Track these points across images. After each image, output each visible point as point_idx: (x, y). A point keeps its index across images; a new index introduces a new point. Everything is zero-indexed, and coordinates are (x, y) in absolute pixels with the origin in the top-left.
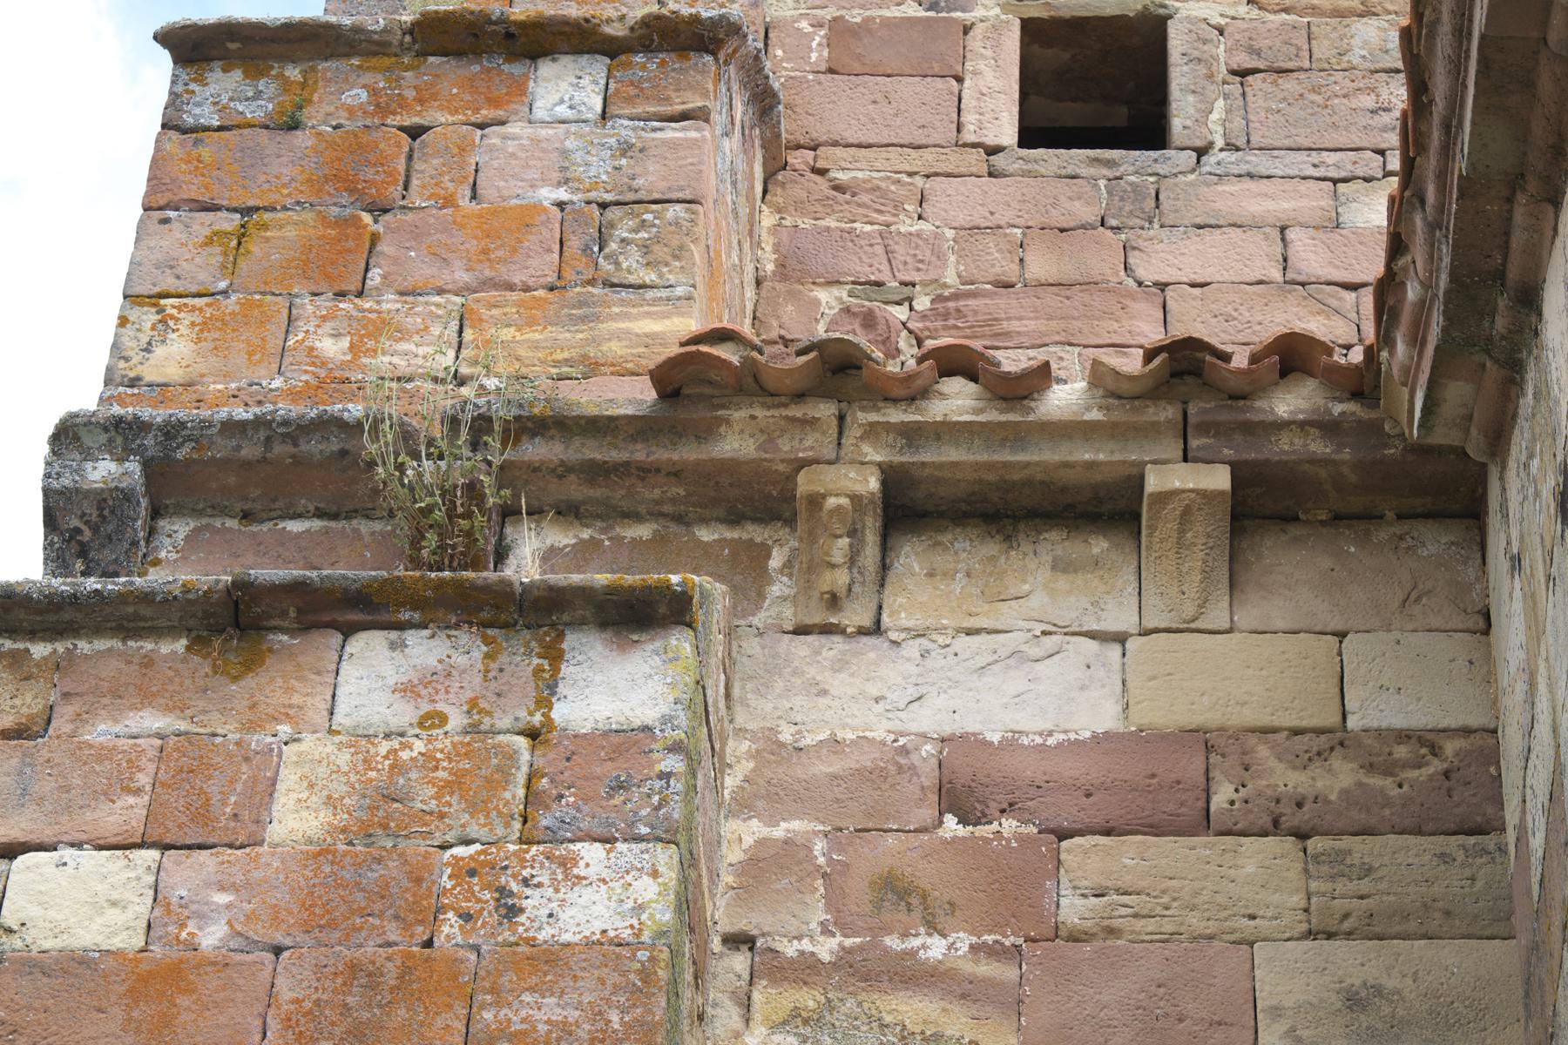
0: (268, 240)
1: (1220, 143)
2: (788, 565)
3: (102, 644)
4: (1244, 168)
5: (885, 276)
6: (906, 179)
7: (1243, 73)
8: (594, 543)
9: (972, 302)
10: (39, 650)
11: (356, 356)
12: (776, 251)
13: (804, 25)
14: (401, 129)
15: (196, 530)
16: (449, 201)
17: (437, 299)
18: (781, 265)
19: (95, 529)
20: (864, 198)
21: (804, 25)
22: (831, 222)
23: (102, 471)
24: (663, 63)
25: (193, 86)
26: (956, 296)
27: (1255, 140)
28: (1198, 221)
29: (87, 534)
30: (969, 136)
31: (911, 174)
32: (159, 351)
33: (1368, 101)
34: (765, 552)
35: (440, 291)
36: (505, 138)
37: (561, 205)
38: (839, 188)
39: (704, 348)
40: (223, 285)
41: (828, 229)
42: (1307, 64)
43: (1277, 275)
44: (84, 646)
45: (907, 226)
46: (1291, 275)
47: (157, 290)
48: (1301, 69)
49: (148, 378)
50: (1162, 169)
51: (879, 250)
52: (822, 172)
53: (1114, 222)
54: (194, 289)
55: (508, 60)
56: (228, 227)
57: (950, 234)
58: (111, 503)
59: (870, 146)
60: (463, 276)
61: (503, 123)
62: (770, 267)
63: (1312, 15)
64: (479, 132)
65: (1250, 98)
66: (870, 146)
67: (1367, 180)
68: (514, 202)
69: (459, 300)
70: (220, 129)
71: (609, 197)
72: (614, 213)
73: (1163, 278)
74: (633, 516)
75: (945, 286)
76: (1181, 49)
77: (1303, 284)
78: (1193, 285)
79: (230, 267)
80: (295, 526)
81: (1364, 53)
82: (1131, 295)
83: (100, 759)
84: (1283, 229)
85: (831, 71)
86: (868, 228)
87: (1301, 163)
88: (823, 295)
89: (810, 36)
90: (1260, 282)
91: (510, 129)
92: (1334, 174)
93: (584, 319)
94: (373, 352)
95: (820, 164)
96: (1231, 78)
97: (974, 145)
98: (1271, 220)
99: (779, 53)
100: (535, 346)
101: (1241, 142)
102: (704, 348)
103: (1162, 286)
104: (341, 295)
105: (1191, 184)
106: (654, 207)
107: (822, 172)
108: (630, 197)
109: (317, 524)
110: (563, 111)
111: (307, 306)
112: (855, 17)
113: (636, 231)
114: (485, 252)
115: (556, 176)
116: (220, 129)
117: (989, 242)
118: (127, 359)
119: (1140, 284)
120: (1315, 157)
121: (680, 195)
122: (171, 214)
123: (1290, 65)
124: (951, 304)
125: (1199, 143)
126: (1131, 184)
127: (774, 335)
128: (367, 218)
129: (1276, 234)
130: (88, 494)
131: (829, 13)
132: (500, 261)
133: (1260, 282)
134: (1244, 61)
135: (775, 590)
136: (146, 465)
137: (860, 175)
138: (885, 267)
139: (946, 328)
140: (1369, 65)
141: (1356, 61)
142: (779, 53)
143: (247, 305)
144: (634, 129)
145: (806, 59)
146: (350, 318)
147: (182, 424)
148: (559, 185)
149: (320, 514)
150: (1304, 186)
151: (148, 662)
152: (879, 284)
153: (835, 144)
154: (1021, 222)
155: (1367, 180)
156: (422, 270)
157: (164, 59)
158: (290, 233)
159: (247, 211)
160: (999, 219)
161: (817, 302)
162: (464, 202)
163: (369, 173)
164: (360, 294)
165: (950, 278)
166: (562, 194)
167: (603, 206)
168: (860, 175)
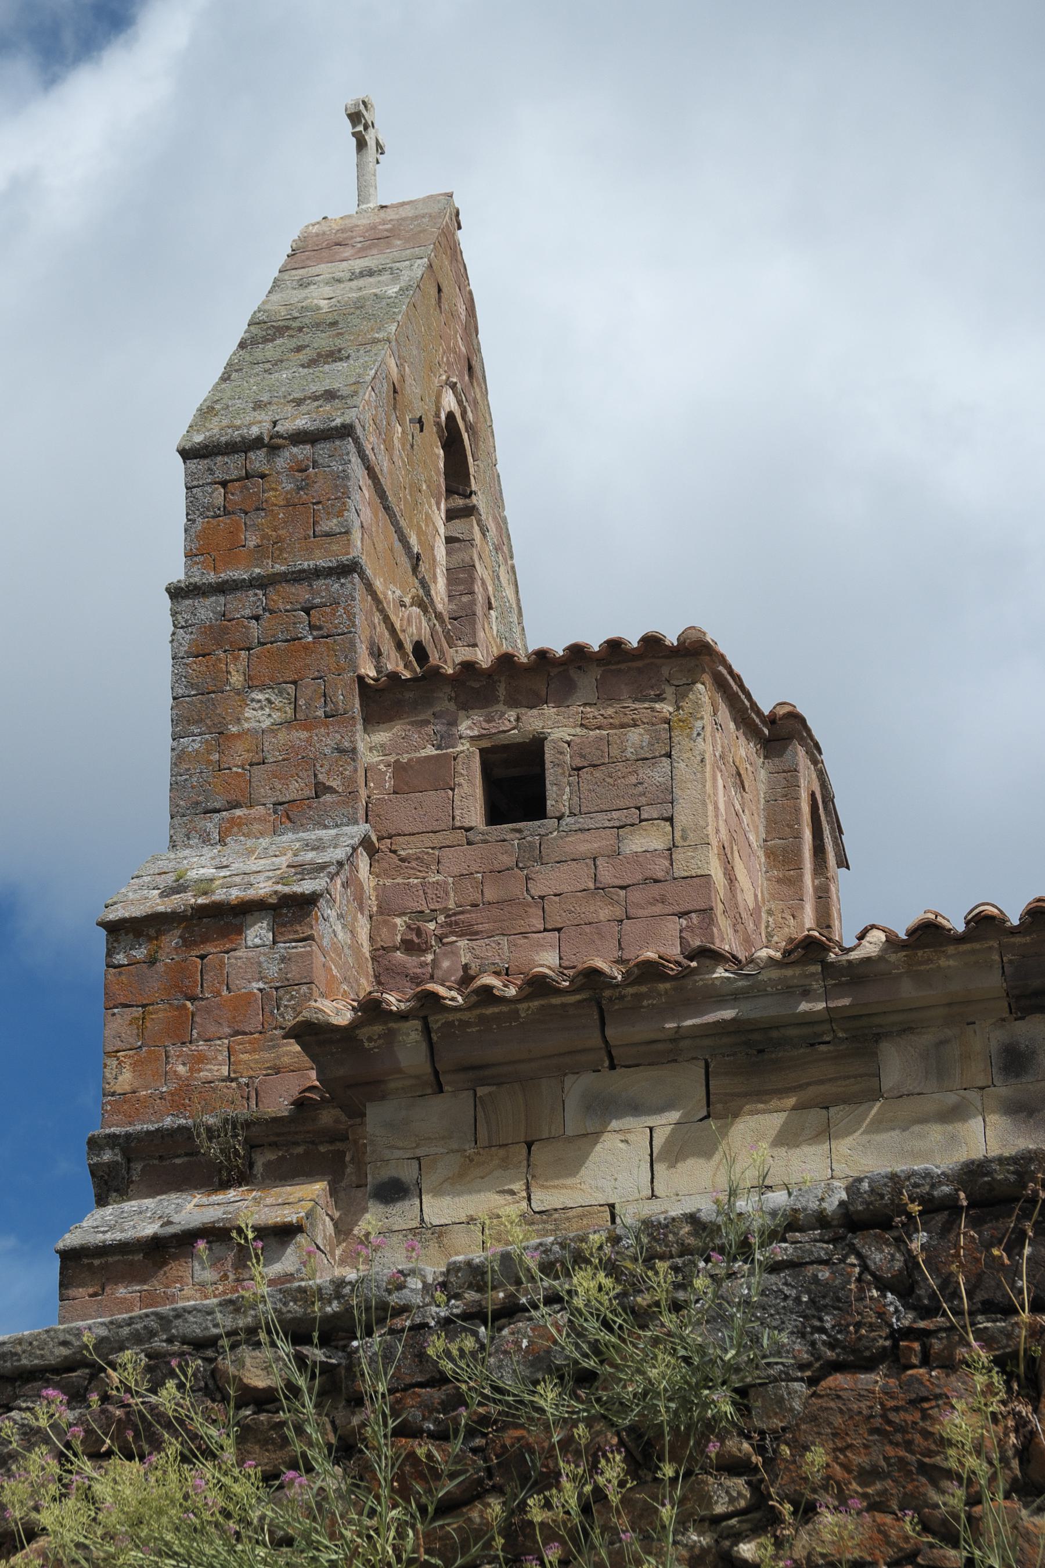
0: (153, 1019)
1: (567, 813)
2: (352, 1159)
3: (116, 1258)
4: (578, 826)
5: (424, 908)
6: (431, 851)
7: (579, 769)
8: (283, 1157)
9: (461, 917)
10: (96, 1262)
11: (192, 1074)
12: (377, 900)
13: (382, 767)
14: (197, 957)
15: (144, 1166)
16: (218, 994)
17: (218, 1042)
18: (379, 907)
19: (109, 1175)
20: (414, 864)
21: (382, 767)
22: (399, 880)
23: (107, 1156)
24: (294, 913)
25: (115, 945)
26: (455, 914)
27: (584, 809)
28: (557, 859)
29: (106, 1177)
30: (458, 824)
31: (433, 848)
32: (120, 1078)
33: (633, 779)
34: (342, 1154)
35: (220, 1038)
36: (236, 959)
37: (260, 990)
38: (402, 860)
39: (307, 1094)
40: (139, 1044)
41: (398, 884)
42: (606, 760)
43: (591, 885)
44: (110, 1260)
45: (434, 878)
46: (598, 885)
47: (115, 1049)
48: (603, 764)
49: (119, 1091)
50: (542, 831)
51: (421, 892)
52: (394, 852)
53: (521, 865)
54: (129, 1047)
55: (234, 917)
56: (136, 1015)
57: (451, 880)
58: (112, 1166)
59: (414, 834)
60: (228, 1030)
61: (235, 950)
62: (375, 909)
63: (610, 729)
64: (226, 956)
65: (581, 784)
66: (414, 834)
67: (632, 825)
68: (243, 990)
69: (226, 1041)
70: (128, 965)
71: (278, 984)
72: (281, 992)
73: (542, 894)
74: (296, 1144)
75: (450, 909)
76: (550, 759)
77: (603, 889)
78: (555, 895)
79: (141, 1035)
80: (178, 1161)
81: (632, 750)
82: (529, 905)
83: (121, 1303)
84: (594, 859)
85: (395, 793)
86: (416, 881)
87: (602, 820)
88: (398, 921)
89: (384, 773)
90: (584, 890)
91: (238, 954)
92: (617, 824)
93: (274, 1047)
94: (200, 1070)
95: (394, 847)
96: (572, 773)
97: (460, 828)
98: (589, 855)
99: (372, 785)
100: (256, 1062)
101: (577, 812)
102: (307, 1094)
103: (542, 898)
104: (184, 1043)
105: (554, 839)
106: (296, 987)
107: (394, 852)
108: (287, 983)
109: (186, 1159)
110: (257, 941)
111: (171, 1049)
112: (404, 759)
113: (289, 1001)
114: (234, 1018)
115: (257, 976)
116: (128, 965)
117: (467, 882)
118: (109, 1084)
119: (533, 898)
120: (609, 816)
121: (305, 981)
122: (116, 1010)
123: (598, 762)
124: (453, 918)
125: (558, 814)
126: (530, 842)
127: (379, 946)
128: (188, 1004)
129: (590, 862)
130: (104, 1164)
131: (392, 759)
132: (241, 1021)
133: (584, 890)
134: (578, 762)
135: (348, 1170)
136: (122, 1150)
137: (410, 851)
138: (424, 902)
139: (451, 932)
140: (634, 757)
141: (629, 755)
142: (372, 785)
143: (149, 1052)
144: (286, 948)
145: (384, 787)
146: (188, 1055)
147: (131, 1134)
148: (259, 981)
149: (187, 1155)
150: (603, 833)
151: (132, 1263)
152: (422, 912)
153: (400, 835)
154: (481, 870)
155: (632, 825)
156: (212, 1029)
157: (103, 933)
158: (161, 1015)
159: (144, 1006)
160: (473, 869)
161: (395, 925)
162: (225, 993)
163: (186, 982)
164: (191, 1042)
165: (451, 905)
166: (261, 985)
167: (277, 988)
168: (410, 851)
